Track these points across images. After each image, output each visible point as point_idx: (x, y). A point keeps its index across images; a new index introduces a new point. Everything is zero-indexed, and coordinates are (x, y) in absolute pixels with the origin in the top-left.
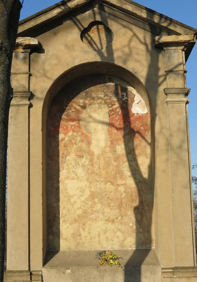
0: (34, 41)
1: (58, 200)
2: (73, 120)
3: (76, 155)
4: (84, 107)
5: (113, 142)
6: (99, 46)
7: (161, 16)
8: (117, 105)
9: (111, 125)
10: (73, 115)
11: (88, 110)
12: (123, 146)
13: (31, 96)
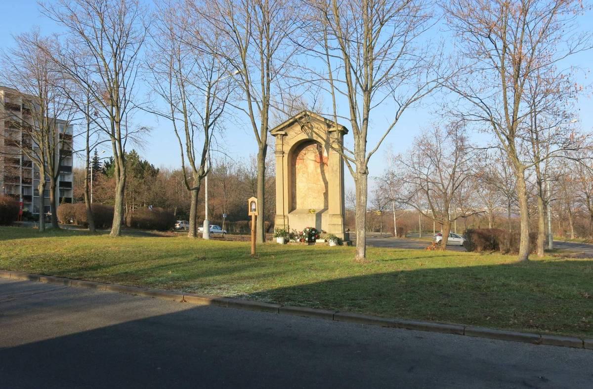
0: (283, 133)
1: (296, 190)
2: (301, 159)
3: (5, 185)
4: (305, 154)
5: (316, 168)
6: (58, 114)
7: (329, 120)
8: (318, 153)
9: (316, 161)
10: (301, 158)
11: (307, 155)
12: (320, 169)
13: (283, 153)
